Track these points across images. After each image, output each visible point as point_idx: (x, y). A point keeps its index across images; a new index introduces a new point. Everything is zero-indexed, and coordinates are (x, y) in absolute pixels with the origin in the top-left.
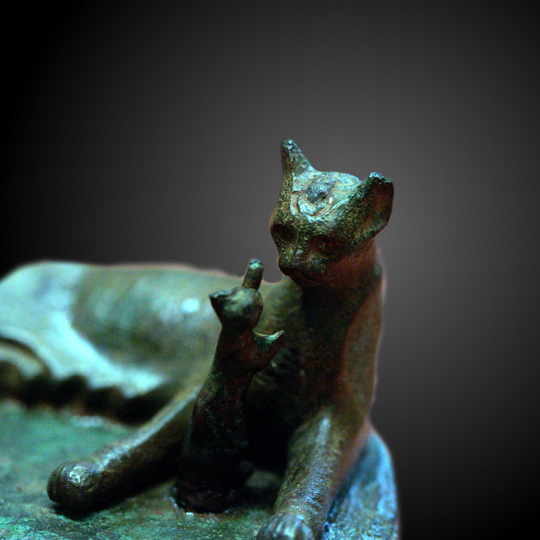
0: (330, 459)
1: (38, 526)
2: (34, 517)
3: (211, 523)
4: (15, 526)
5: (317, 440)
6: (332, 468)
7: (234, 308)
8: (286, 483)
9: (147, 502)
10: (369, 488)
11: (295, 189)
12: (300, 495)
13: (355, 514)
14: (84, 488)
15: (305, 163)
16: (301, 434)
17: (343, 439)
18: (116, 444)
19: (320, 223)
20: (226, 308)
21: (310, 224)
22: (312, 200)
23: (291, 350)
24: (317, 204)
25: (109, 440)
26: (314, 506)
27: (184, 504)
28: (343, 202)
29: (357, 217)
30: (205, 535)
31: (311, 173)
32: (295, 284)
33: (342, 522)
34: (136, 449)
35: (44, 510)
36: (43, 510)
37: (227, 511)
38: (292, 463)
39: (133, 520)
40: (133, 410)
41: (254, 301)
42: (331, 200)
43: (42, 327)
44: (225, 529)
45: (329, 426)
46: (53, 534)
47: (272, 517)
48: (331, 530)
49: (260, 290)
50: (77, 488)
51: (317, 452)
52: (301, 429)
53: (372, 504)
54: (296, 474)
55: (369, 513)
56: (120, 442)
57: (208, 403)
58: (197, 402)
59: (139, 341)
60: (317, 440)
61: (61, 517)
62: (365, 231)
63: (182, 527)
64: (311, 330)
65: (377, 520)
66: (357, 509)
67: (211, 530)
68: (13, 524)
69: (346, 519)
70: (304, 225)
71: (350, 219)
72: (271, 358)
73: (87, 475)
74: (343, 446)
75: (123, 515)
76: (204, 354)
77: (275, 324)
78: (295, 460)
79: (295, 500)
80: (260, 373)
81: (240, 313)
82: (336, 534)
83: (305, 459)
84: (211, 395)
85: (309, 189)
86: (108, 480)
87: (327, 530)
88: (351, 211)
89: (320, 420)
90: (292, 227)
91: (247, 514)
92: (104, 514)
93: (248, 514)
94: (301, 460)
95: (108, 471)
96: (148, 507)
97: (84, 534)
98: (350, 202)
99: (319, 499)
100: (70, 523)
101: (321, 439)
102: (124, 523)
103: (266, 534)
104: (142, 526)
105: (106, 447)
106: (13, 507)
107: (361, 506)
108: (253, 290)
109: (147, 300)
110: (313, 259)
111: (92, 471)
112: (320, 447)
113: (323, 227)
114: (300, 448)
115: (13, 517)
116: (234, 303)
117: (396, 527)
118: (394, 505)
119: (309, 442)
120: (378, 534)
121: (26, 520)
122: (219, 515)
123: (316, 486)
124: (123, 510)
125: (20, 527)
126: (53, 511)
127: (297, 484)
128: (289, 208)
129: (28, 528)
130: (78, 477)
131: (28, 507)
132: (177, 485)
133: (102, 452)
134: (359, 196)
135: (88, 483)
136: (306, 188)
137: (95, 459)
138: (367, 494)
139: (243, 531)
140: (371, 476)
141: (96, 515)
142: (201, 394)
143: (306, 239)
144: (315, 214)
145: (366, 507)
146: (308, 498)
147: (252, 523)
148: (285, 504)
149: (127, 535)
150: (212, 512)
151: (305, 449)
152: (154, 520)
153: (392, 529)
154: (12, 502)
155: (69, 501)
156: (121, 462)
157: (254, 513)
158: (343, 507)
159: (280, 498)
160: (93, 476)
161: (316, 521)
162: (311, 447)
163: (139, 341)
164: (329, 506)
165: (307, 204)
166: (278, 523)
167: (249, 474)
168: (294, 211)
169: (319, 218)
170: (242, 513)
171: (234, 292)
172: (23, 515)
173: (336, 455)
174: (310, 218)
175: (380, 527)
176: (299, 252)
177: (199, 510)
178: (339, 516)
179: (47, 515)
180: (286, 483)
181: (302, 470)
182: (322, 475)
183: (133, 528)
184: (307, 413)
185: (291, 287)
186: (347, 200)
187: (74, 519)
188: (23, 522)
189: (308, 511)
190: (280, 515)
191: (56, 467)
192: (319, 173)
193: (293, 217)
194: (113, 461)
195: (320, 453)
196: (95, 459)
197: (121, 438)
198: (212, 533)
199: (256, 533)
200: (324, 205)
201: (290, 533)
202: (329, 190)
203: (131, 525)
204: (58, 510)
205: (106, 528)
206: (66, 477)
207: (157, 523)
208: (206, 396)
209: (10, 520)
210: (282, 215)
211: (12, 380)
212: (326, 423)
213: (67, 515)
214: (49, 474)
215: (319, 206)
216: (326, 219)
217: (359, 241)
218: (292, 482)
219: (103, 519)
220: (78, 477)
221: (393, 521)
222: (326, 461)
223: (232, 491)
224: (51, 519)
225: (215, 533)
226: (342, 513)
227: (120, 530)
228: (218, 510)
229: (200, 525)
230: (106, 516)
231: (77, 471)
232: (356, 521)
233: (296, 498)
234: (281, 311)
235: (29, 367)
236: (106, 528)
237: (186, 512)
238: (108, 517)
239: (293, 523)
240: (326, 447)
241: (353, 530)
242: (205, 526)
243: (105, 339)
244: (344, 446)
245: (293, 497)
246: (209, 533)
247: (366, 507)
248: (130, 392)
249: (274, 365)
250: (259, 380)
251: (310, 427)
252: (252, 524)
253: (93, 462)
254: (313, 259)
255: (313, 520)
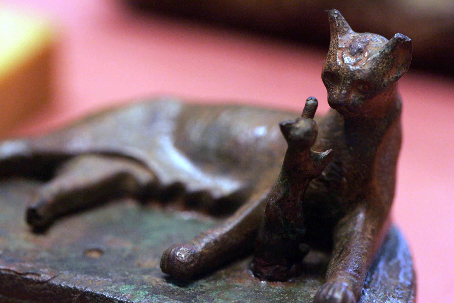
7: (297, 133)
11: (340, 46)
19: (359, 71)
22: (353, 54)
54: (341, 253)
70: (347, 73)
113: (361, 73)
116: (297, 129)
144: (355, 64)
187: (179, 286)
235: (143, 176)
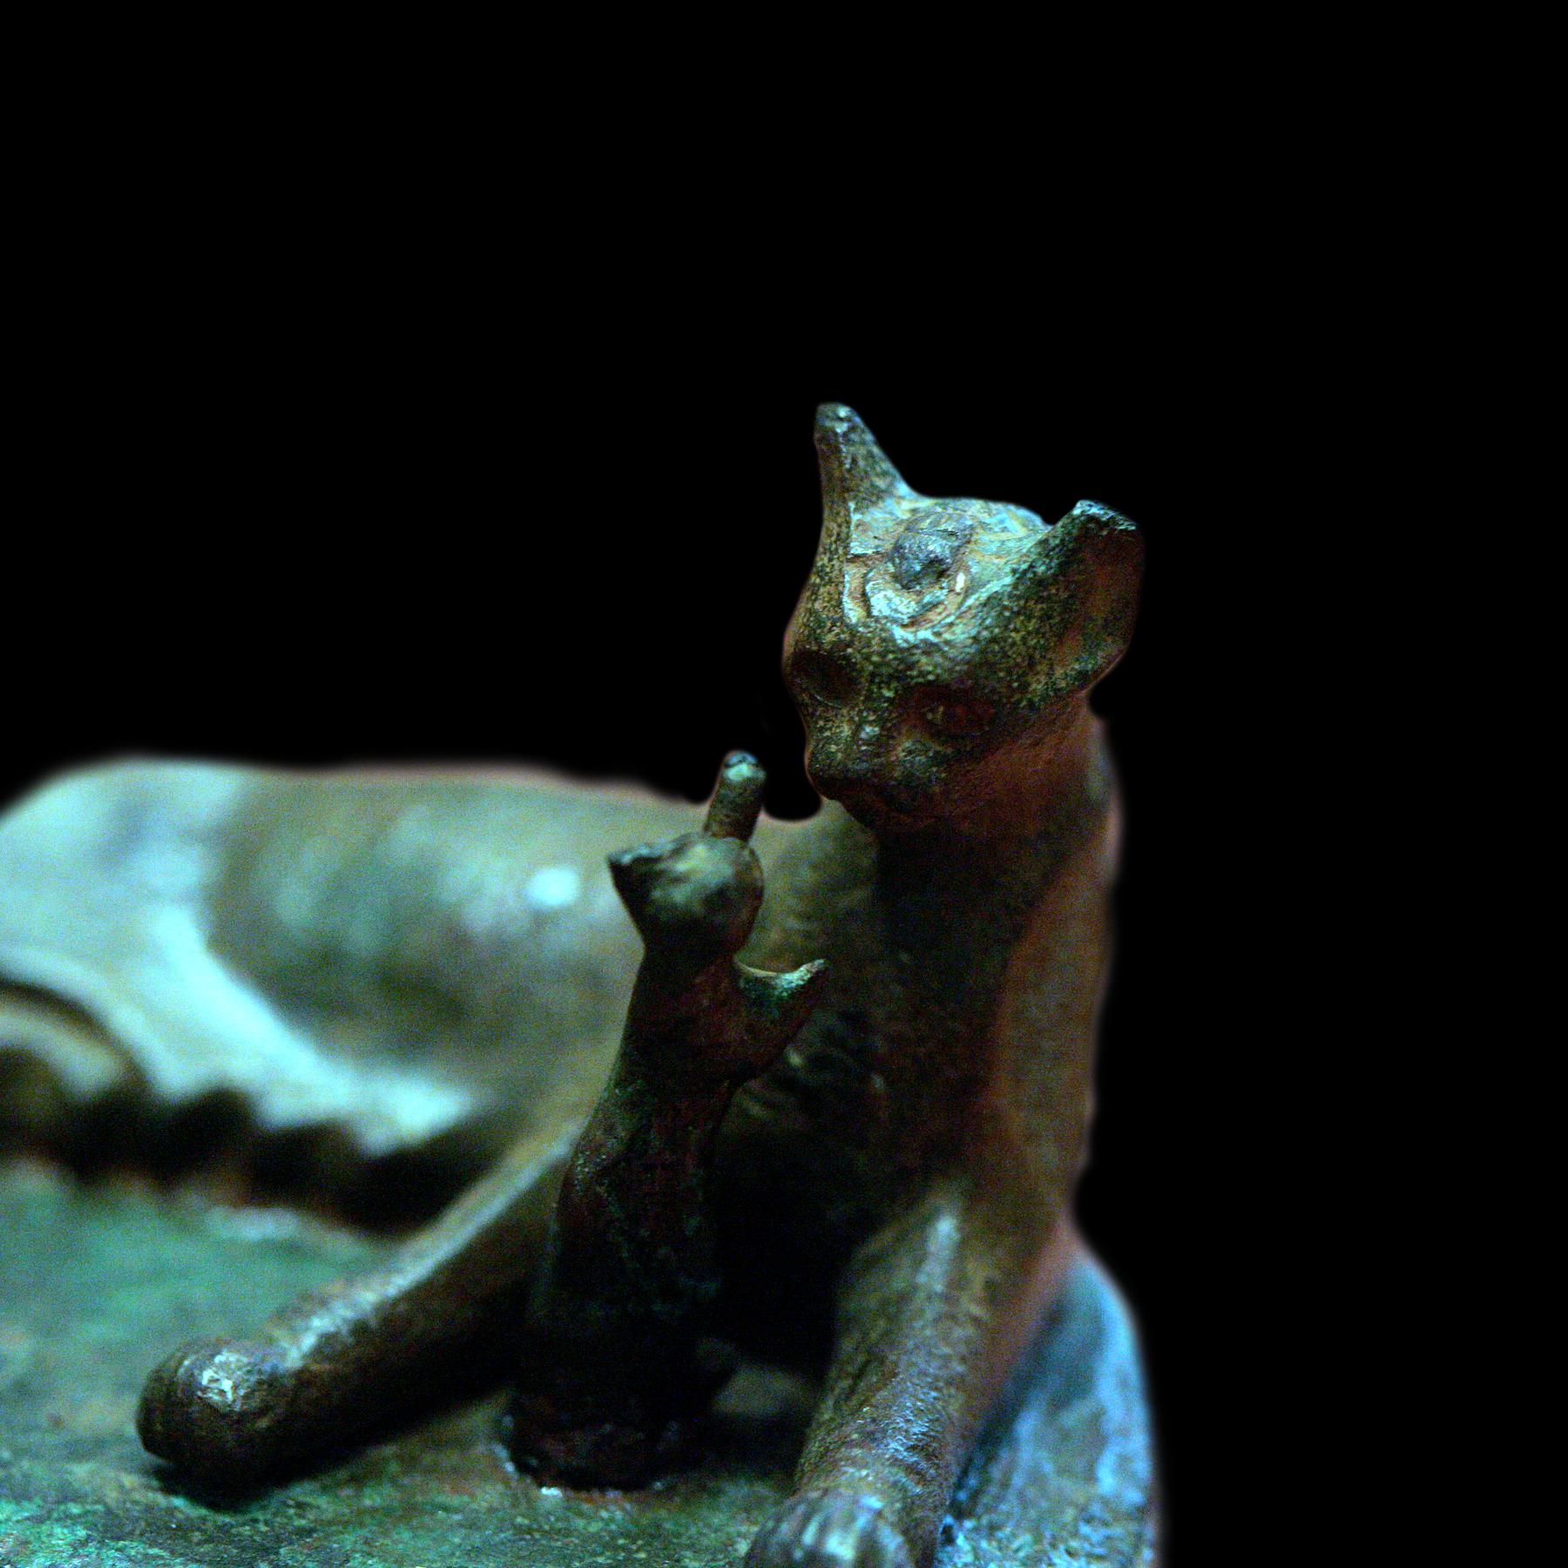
0: (958, 1332)
1: (111, 1527)
2: (99, 1501)
3: (612, 1520)
4: (45, 1528)
5: (922, 1279)
6: (963, 1359)
7: (679, 895)
8: (830, 1403)
9: (428, 1459)
10: (1072, 1418)
11: (856, 549)
12: (870, 1438)
13: (1031, 1492)
14: (243, 1417)
15: (885, 474)
16: (874, 1261)
17: (997, 1275)
18: (336, 1288)
19: (929, 648)
20: (657, 894)
21: (902, 650)
22: (906, 582)
23: (846, 1017)
24: (919, 593)
25: (317, 1277)
26: (911, 1469)
27: (534, 1462)
28: (995, 587)
29: (1037, 631)
30: (594, 1554)
31: (904, 501)
32: (857, 825)
33: (994, 1517)
34: (395, 1302)
35: (129, 1480)
36: (124, 1481)
37: (658, 1485)
38: (847, 1345)
39: (388, 1511)
40: (386, 1191)
41: (738, 875)
42: (961, 581)
43: (122, 948)
44: (654, 1535)
45: (956, 1237)
46: (154, 1551)
47: (789, 1502)
48: (960, 1540)
49: (755, 842)
50: (224, 1416)
51: (920, 1313)
52: (874, 1246)
53: (1079, 1465)
54: (859, 1375)
55: (1072, 1488)
56: (350, 1282)
57: (605, 1172)
58: (573, 1167)
59: (405, 990)
60: (922, 1279)
61: (178, 1502)
62: (1059, 672)
63: (530, 1531)
64: (904, 957)
65: (1096, 1509)
66: (1036, 1478)
67: (613, 1538)
68: (38, 1520)
69: (1004, 1507)
70: (883, 655)
71: (1016, 637)
72: (788, 1040)
73: (254, 1378)
74: (995, 1295)
75: (358, 1496)
76: (593, 1027)
77: (798, 940)
78: (857, 1335)
79: (857, 1452)
80: (754, 1084)
81: (698, 909)
82: (976, 1551)
83: (886, 1334)
84: (612, 1146)
85: (898, 548)
86: (314, 1393)
87: (949, 1538)
88: (1018, 613)
89: (928, 1220)
90: (847, 658)
91: (719, 1492)
92: (302, 1491)
93: (720, 1491)
94: (874, 1336)
95: (315, 1367)
96: (429, 1471)
97: (243, 1549)
98: (1015, 586)
99: (925, 1448)
100: (204, 1520)
101: (933, 1275)
102: (359, 1518)
103: (773, 1550)
104: (412, 1528)
105: (307, 1297)
106: (39, 1471)
107: (1048, 1468)
108: (734, 842)
109: (425, 872)
110: (909, 752)
111: (267, 1367)
112: (929, 1298)
113: (938, 658)
114: (872, 1302)
115: (38, 1500)
116: (678, 880)
117: (1151, 1530)
118: (1143, 1466)
119: (898, 1283)
120: (1099, 1551)
121: (75, 1509)
122: (636, 1495)
123: (919, 1413)
124: (358, 1481)
125: (58, 1530)
126: (155, 1483)
127: (862, 1405)
128: (840, 603)
129: (82, 1533)
130: (227, 1385)
131: (80, 1471)
132: (514, 1409)
133: (297, 1311)
134: (1041, 569)
135: (255, 1403)
136: (888, 546)
137: (277, 1333)
138: (1066, 1435)
139: (706, 1542)
140: (1078, 1383)
141: (279, 1496)
142: (584, 1145)
143: (888, 694)
144: (914, 622)
145: (1062, 1471)
146: (895, 1446)
147: (733, 1517)
148: (828, 1463)
149: (370, 1555)
150: (617, 1486)
151: (885, 1303)
152: (446, 1509)
153: (1139, 1537)
154: (36, 1457)
155: (202, 1455)
156: (351, 1340)
157: (737, 1491)
158: (996, 1472)
159: (814, 1447)
160: (270, 1383)
161: (918, 1514)
162: (904, 1298)
163: (405, 990)
164: (955, 1469)
165: (890, 593)
166: (807, 1519)
167: (723, 1377)
168: (853, 612)
169: (925, 634)
170: (703, 1488)
171: (680, 849)
172: (68, 1494)
173: (976, 1321)
174: (899, 634)
175: (1104, 1531)
176: (869, 731)
177: (579, 1481)
178: (985, 1499)
179: (136, 1496)
180: (830, 1403)
181: (876, 1364)
182: (936, 1378)
183: (386, 1534)
184: (892, 1200)
185: (846, 833)
186: (1008, 580)
187: (214, 1506)
188: (68, 1516)
189: (895, 1484)
190: (814, 1495)
191: (162, 1357)
192: (926, 503)
193: (852, 630)
194: (327, 1339)
195: (929, 1315)
196: (277, 1333)
197: (353, 1273)
198: (617, 1548)
199: (743, 1547)
200: (941, 594)
201: (841, 1547)
202: (956, 551)
203: (380, 1524)
204: (169, 1481)
205: (309, 1532)
206: (192, 1384)
207: (457, 1517)
208: (597, 1149)
209: (29, 1509)
210: (820, 623)
211: (34, 1103)
212: (945, 1228)
213: (194, 1497)
214: (142, 1376)
215: (927, 599)
216: (947, 636)
217: (1043, 699)
218: (848, 1398)
219: (300, 1506)
220: (227, 1385)
221: (1140, 1513)
222: (946, 1339)
223: (674, 1426)
224: (149, 1508)
225: (623, 1548)
226: (994, 1489)
227: (349, 1540)
228: (632, 1482)
229: (580, 1523)
230: (309, 1499)
231: (224, 1366)
232: (1032, 1514)
233: (860, 1445)
234: (817, 904)
235: (83, 1067)
236: (309, 1532)
237: (541, 1485)
238: (315, 1501)
239: (852, 1518)
240: (947, 1298)
241: (1025, 1539)
242: (594, 1527)
243: (306, 985)
244: (999, 1295)
245: (851, 1444)
246: (606, 1546)
247: (1062, 1471)
248: (377, 1139)
249: (795, 1059)
250: (752, 1104)
251: (899, 1240)
252: (731, 1523)
253: (270, 1341)
254: (909, 752)
255: (908, 1509)
